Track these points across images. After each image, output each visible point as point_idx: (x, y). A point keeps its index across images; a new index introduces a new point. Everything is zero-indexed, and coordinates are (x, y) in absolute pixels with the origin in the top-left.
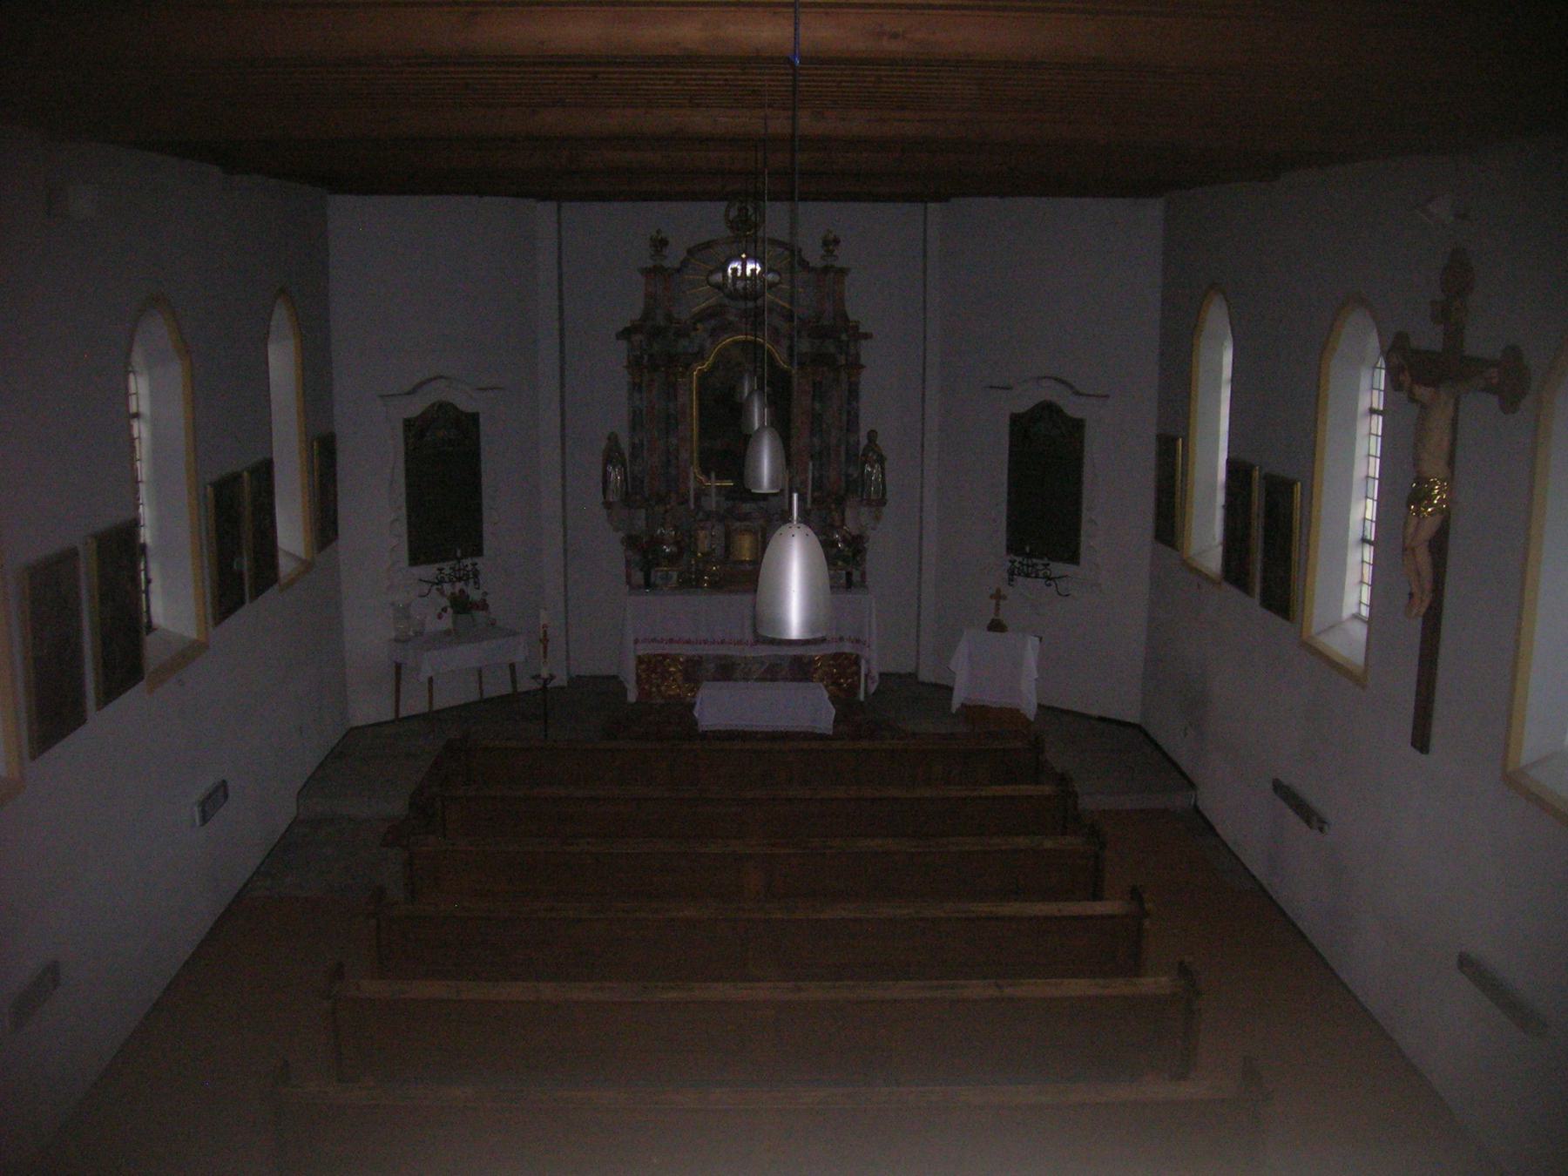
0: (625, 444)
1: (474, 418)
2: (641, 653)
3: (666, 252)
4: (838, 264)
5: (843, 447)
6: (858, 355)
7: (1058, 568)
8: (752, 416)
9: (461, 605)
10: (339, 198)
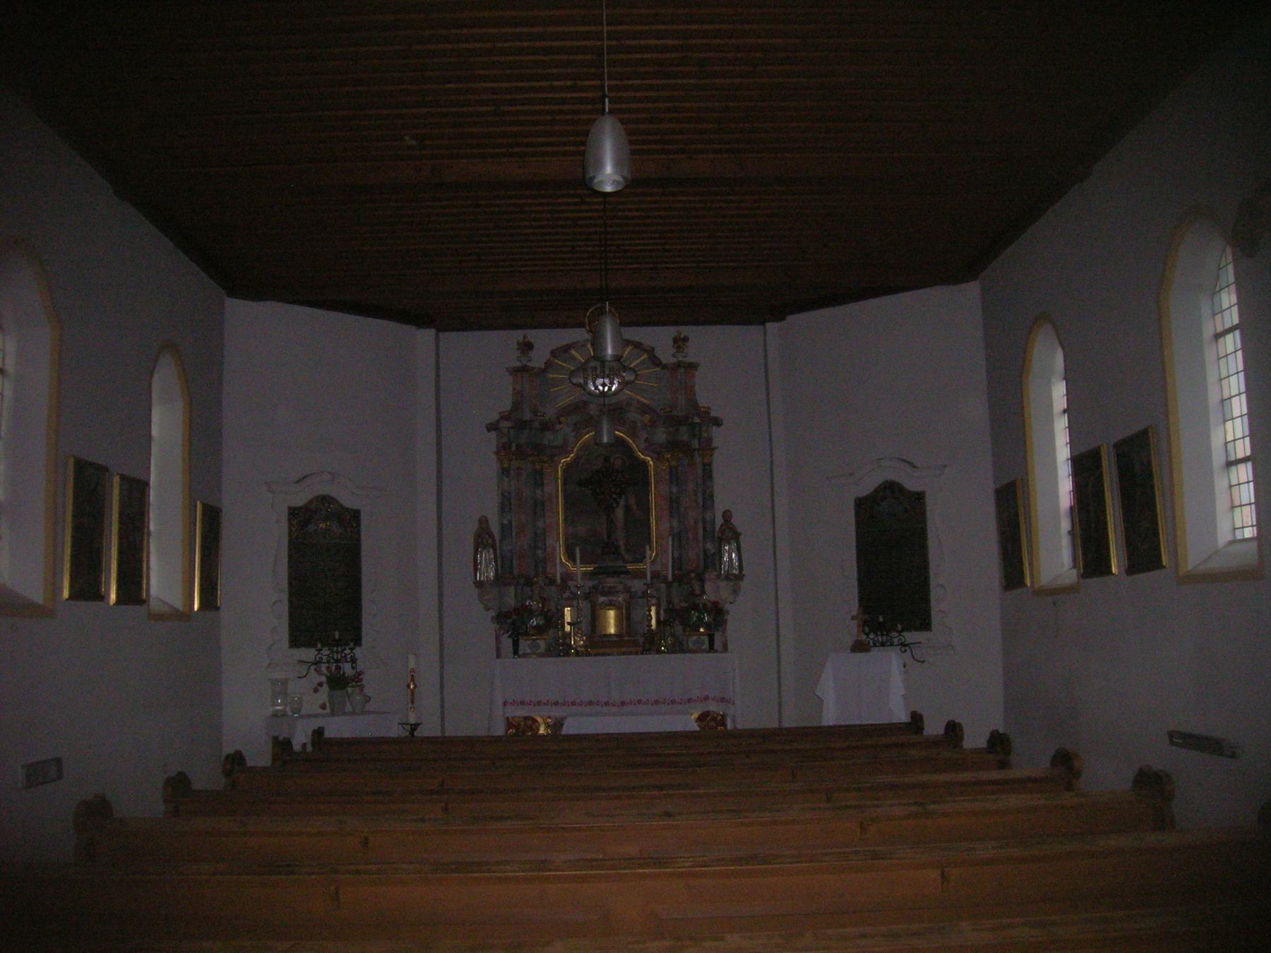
0: (495, 528)
1: (356, 515)
2: (509, 715)
3: (532, 354)
4: (688, 360)
5: (700, 526)
6: (710, 440)
7: (909, 636)
8: (605, 339)
9: (337, 682)
10: (235, 301)
